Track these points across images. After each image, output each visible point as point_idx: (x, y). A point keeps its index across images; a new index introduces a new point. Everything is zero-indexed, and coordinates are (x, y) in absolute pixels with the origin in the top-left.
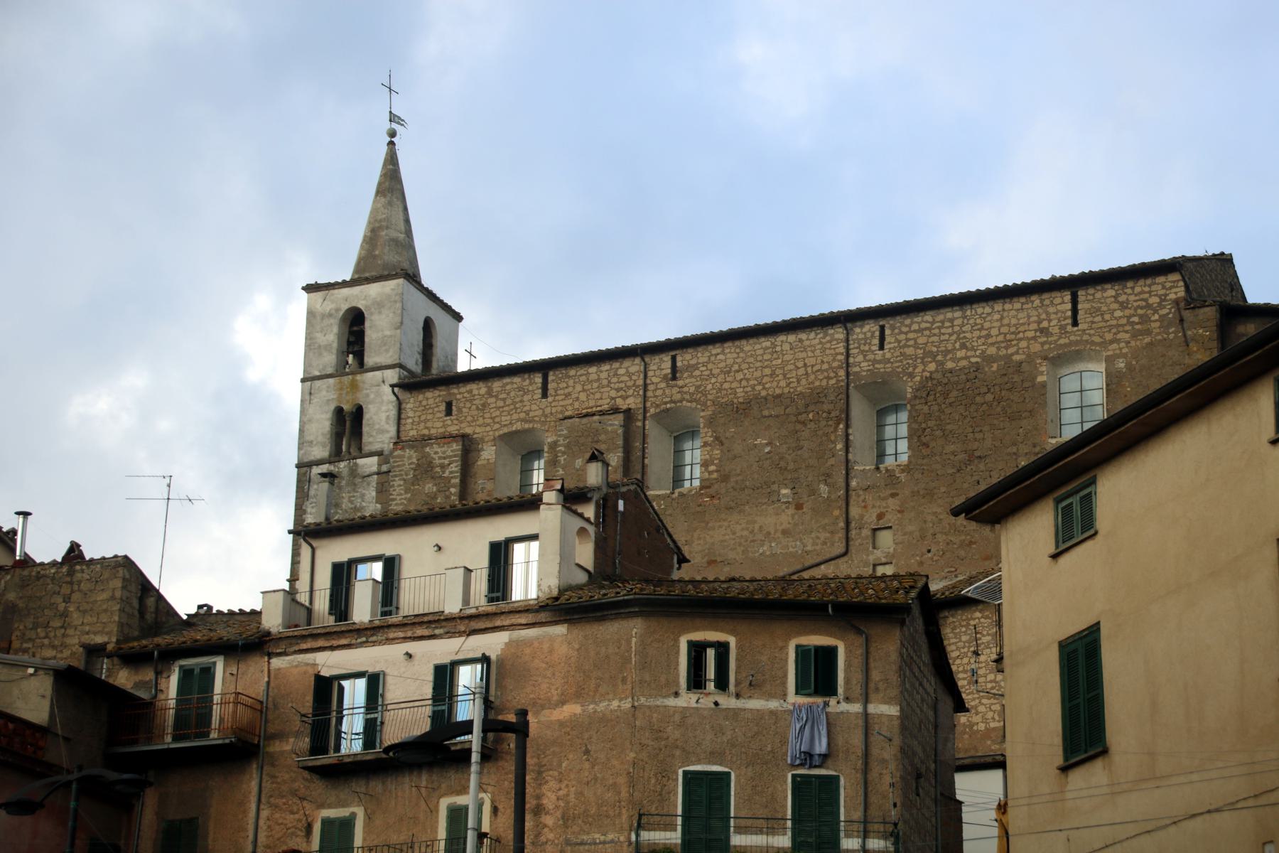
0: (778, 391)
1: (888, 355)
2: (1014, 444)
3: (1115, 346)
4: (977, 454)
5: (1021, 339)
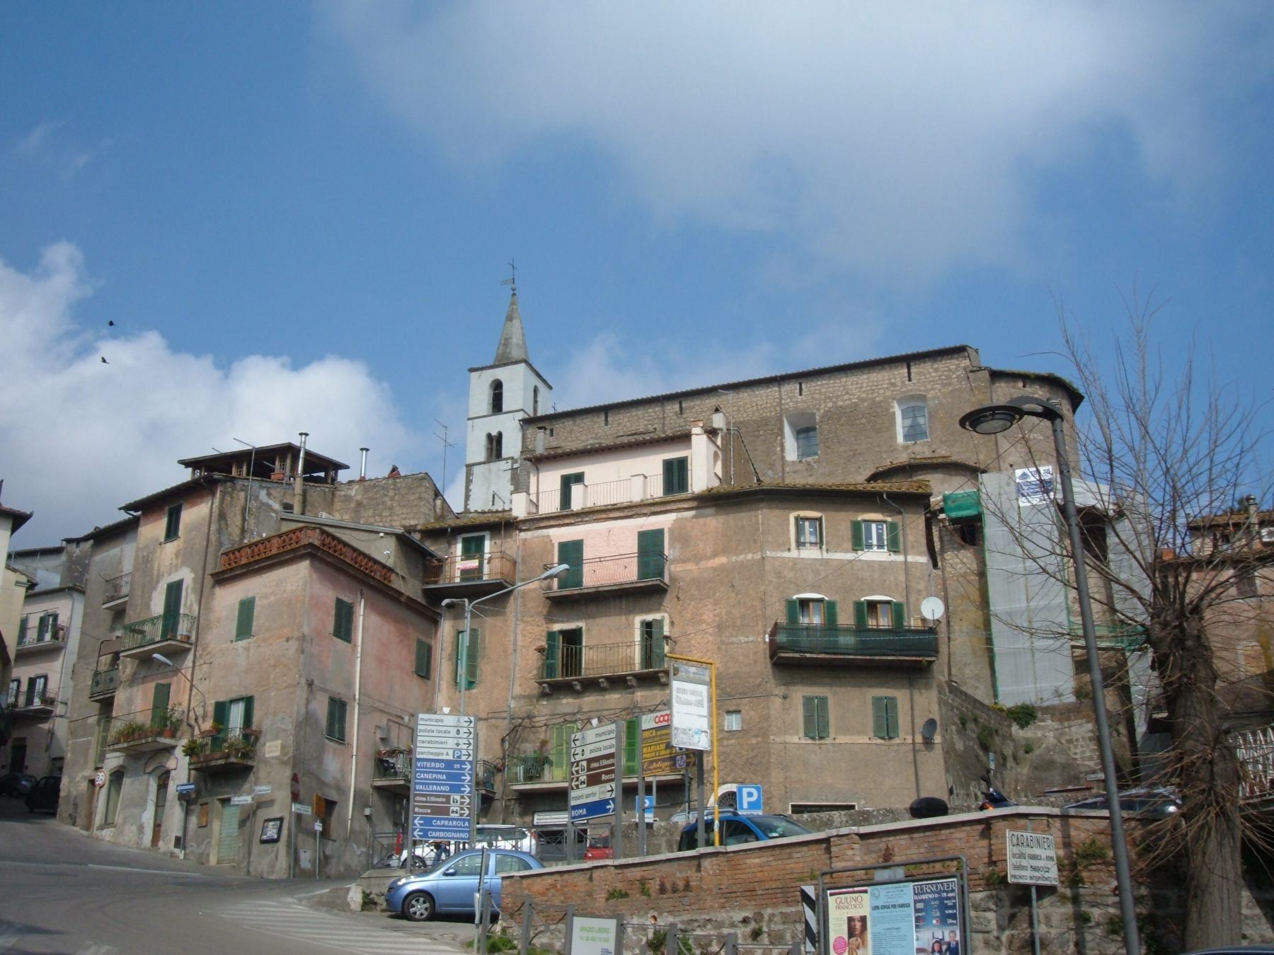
0: (742, 419)
1: (805, 399)
2: (879, 446)
3: (932, 392)
4: (858, 451)
5: (879, 389)
